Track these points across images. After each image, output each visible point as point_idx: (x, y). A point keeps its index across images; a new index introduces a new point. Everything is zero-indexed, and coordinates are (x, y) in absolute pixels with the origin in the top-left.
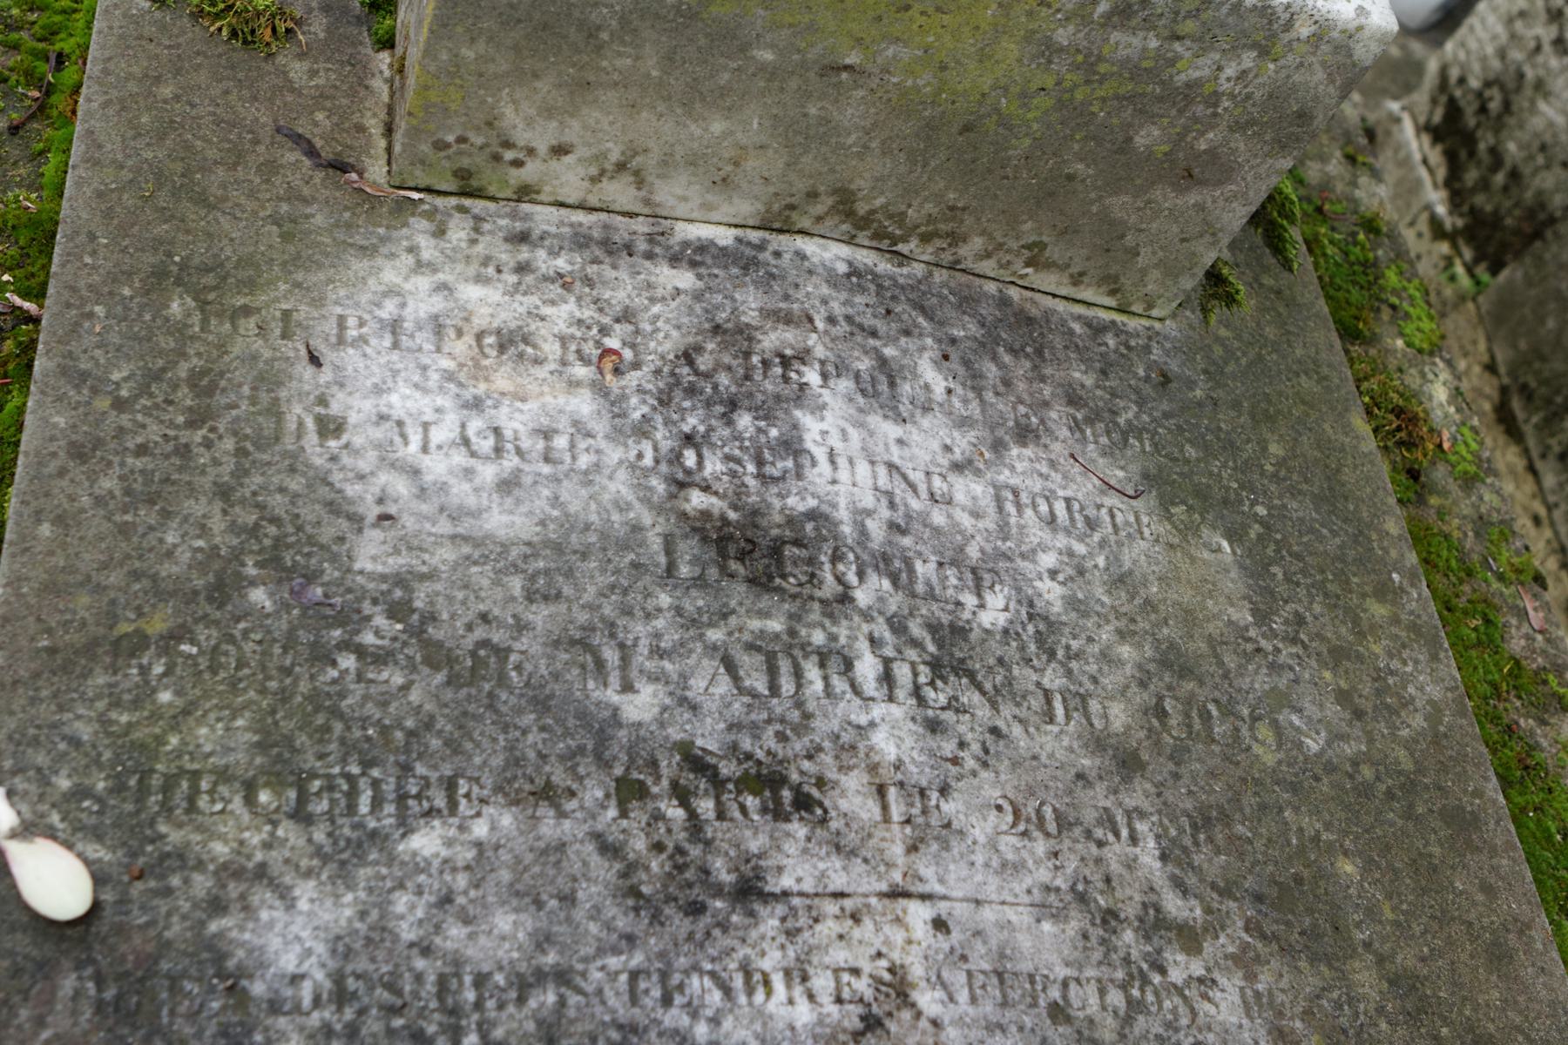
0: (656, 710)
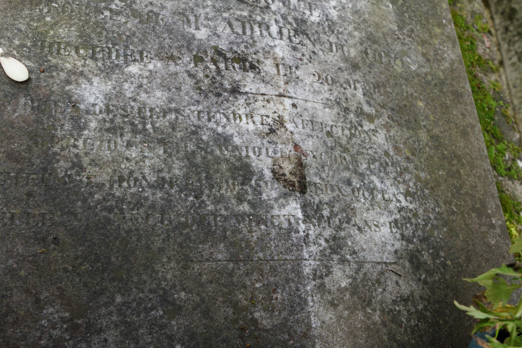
0: (207, 36)
